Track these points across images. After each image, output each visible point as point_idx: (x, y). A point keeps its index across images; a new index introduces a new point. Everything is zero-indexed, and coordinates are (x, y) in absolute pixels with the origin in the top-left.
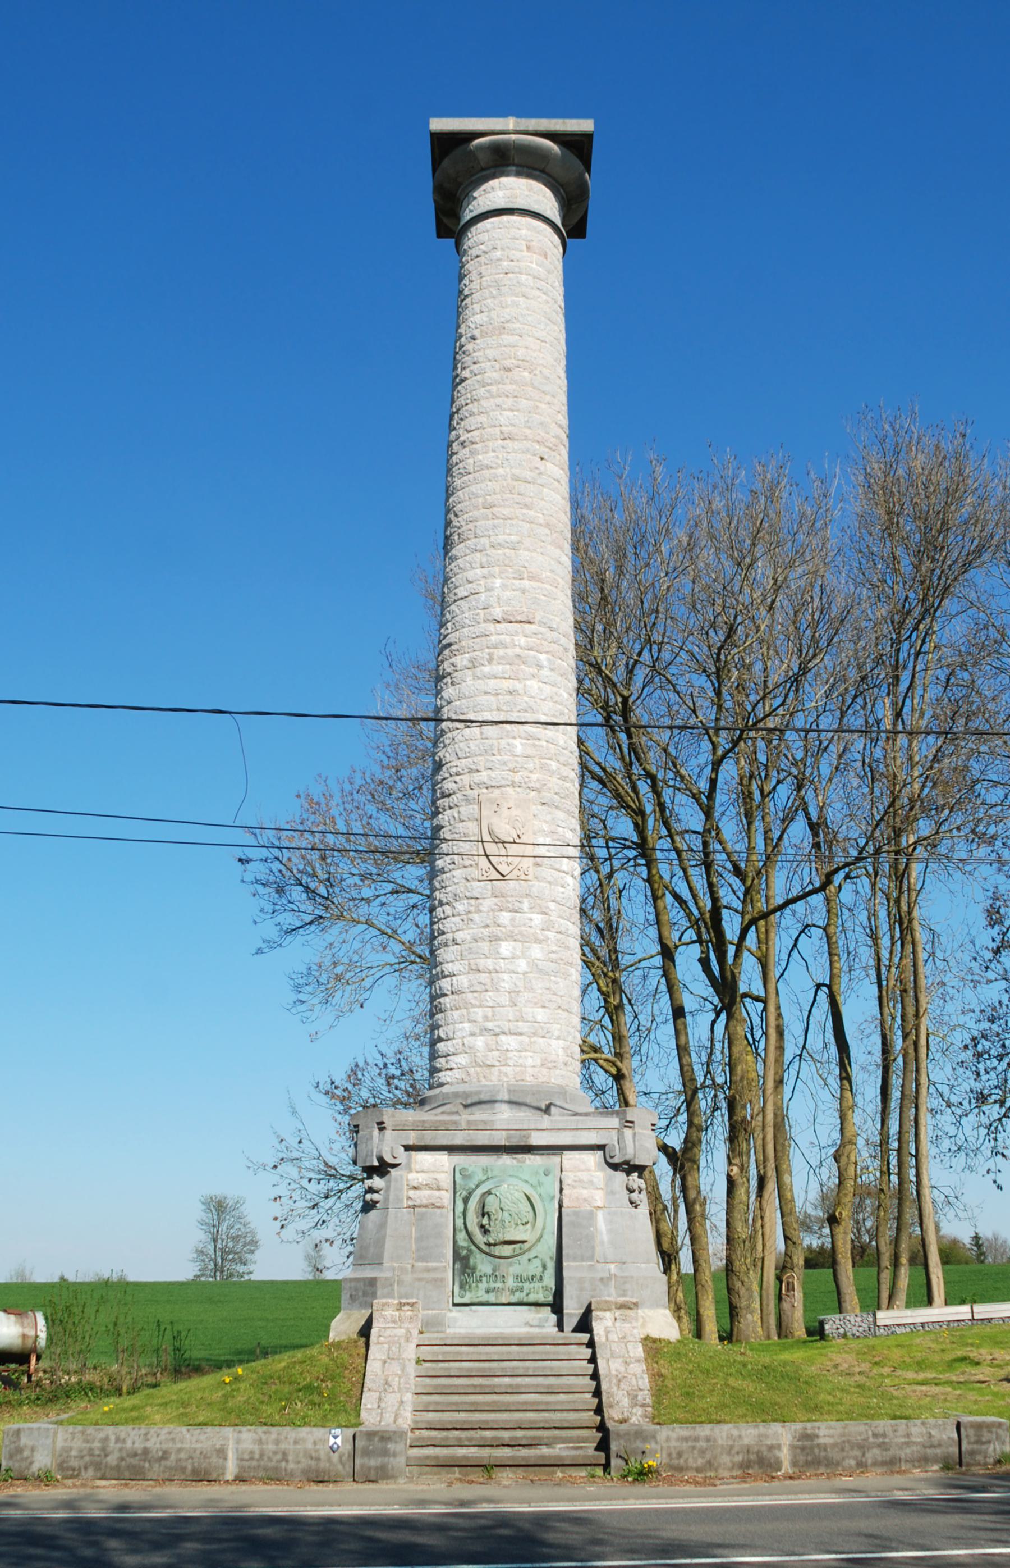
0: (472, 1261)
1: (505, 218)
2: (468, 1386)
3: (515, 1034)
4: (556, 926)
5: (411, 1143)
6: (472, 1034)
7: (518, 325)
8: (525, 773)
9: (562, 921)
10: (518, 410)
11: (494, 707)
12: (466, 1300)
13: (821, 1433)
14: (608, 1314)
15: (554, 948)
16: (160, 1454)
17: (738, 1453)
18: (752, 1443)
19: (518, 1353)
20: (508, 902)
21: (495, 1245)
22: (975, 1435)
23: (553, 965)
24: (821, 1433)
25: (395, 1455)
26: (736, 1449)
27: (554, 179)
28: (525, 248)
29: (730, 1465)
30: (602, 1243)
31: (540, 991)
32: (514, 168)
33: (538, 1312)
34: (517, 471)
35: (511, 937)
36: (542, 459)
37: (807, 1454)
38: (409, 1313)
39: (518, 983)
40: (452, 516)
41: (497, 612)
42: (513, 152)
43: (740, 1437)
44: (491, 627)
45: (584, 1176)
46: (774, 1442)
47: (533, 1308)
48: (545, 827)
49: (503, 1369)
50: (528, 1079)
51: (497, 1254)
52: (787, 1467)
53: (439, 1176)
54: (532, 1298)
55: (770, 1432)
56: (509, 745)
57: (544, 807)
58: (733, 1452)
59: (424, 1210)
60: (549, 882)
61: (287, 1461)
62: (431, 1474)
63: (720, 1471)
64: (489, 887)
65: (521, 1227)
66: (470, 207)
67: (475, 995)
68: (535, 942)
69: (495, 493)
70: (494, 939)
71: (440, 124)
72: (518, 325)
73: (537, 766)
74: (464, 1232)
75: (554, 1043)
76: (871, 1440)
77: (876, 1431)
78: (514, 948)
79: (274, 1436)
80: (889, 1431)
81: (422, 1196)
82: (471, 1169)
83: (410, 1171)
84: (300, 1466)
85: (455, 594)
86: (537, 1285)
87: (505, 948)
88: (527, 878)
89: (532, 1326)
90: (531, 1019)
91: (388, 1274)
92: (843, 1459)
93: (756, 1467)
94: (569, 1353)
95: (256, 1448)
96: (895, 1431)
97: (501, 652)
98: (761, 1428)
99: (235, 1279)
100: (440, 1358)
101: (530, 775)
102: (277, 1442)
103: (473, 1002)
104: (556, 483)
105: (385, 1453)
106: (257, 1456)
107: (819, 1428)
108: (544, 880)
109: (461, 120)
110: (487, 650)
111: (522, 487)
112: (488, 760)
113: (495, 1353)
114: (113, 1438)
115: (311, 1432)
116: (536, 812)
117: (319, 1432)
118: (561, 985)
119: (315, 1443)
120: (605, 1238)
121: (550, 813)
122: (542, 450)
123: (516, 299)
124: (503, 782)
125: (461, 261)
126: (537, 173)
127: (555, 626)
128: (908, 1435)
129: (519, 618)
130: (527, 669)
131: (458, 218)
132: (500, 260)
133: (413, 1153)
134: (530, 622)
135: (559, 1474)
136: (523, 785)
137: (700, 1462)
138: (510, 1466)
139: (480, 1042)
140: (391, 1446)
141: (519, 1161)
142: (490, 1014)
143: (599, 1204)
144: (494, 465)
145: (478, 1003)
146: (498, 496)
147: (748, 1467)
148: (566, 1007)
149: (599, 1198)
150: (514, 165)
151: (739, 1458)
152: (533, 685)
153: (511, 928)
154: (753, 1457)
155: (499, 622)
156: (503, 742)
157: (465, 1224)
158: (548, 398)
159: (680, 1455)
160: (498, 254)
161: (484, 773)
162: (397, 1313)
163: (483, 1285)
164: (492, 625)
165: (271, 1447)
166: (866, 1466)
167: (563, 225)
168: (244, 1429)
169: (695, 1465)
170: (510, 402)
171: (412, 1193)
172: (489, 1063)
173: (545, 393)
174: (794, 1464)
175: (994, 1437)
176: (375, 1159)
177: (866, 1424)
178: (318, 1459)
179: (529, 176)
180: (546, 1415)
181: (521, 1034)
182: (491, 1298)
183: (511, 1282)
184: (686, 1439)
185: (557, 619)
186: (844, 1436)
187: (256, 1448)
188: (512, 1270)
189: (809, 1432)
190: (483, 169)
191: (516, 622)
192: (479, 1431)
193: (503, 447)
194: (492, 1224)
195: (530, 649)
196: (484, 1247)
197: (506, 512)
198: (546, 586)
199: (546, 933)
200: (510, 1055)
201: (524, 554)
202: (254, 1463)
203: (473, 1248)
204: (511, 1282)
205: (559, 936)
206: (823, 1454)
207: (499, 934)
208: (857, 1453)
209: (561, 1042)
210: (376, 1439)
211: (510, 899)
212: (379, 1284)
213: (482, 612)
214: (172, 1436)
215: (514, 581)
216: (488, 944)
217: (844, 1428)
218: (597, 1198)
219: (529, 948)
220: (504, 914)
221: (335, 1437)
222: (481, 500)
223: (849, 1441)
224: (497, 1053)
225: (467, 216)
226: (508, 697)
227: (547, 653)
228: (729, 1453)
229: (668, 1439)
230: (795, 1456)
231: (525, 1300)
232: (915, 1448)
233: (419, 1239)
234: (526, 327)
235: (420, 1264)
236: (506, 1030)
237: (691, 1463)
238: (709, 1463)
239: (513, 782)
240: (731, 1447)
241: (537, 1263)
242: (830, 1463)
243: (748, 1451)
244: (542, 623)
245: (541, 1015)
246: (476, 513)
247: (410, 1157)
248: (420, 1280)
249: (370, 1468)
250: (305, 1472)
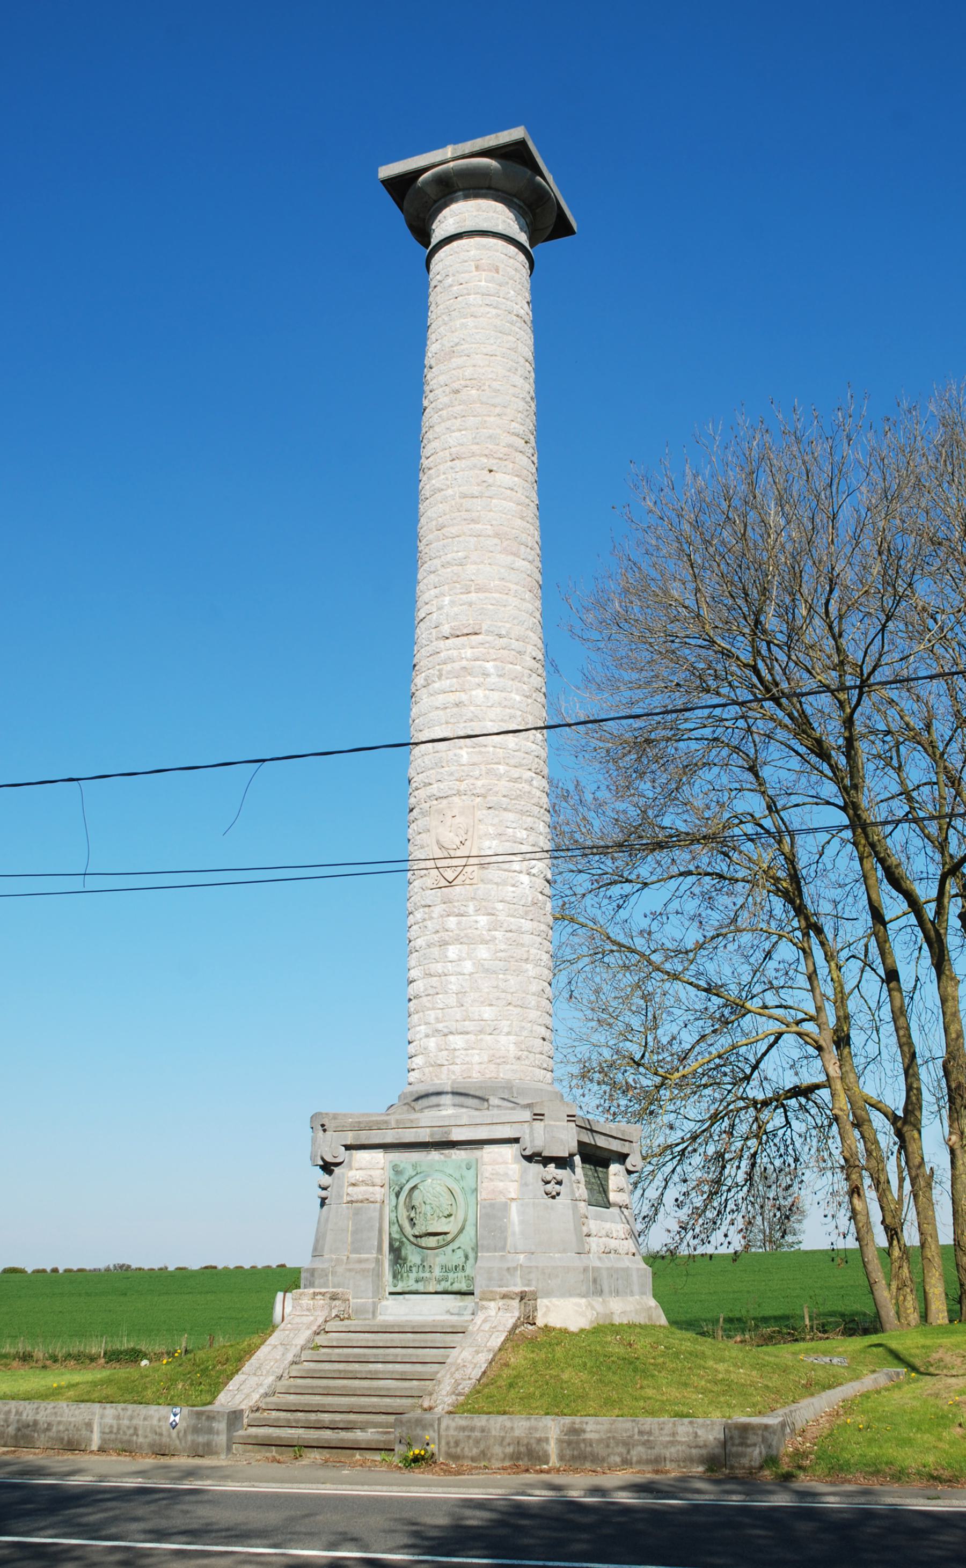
0: (403, 1252)
1: (455, 244)
2: (334, 1371)
3: (461, 1033)
4: (505, 925)
5: (349, 1143)
6: (427, 1036)
7: (466, 346)
8: (472, 781)
9: (512, 920)
10: (465, 429)
11: (443, 721)
12: (398, 1289)
13: (589, 1428)
14: (492, 1304)
15: (503, 947)
16: (46, 1425)
17: (509, 1444)
18: (523, 1435)
19: (401, 1340)
20: (454, 907)
21: (421, 1237)
22: (740, 1437)
23: (502, 963)
24: (589, 1428)
25: (218, 1433)
26: (507, 1440)
27: (503, 192)
28: (474, 269)
29: (501, 1455)
30: (514, 1233)
31: (487, 990)
32: (460, 193)
33: (462, 1300)
34: (464, 489)
35: (458, 940)
36: (491, 471)
37: (573, 1449)
38: (322, 1302)
39: (464, 984)
41: (446, 629)
42: (455, 179)
43: (512, 1428)
44: (442, 644)
45: (501, 1169)
46: (543, 1435)
47: (458, 1296)
48: (491, 830)
49: (375, 1355)
50: (474, 1075)
51: (423, 1245)
52: (554, 1461)
53: (372, 1173)
54: (456, 1287)
55: (541, 1424)
56: (455, 755)
57: (490, 811)
58: (505, 1443)
59: (360, 1205)
60: (496, 883)
61: (137, 1435)
62: (253, 1452)
63: (493, 1461)
64: (439, 894)
65: (444, 1219)
67: (429, 998)
68: (481, 943)
69: (445, 514)
70: (444, 944)
71: (387, 171)
72: (466, 346)
73: (483, 772)
74: (396, 1225)
75: (503, 1039)
76: (636, 1437)
77: (642, 1428)
78: (460, 951)
79: (129, 1413)
80: (655, 1428)
81: (358, 1192)
82: (402, 1166)
83: (351, 1168)
84: (148, 1440)
86: (460, 1274)
87: (453, 951)
88: (472, 882)
89: (452, 1314)
90: (476, 1018)
91: (326, 1265)
92: (608, 1455)
93: (526, 1459)
94: (444, 1342)
95: (114, 1422)
96: (662, 1429)
97: (448, 667)
98: (533, 1420)
99: (785, 1249)
100: (335, 1344)
101: (476, 782)
102: (131, 1418)
103: (428, 1005)
104: (509, 491)
105: (210, 1431)
106: (115, 1430)
107: (587, 1423)
108: (490, 882)
109: (405, 161)
110: (438, 667)
111: (467, 503)
112: (438, 773)
113: (381, 1340)
114: (14, 1411)
115: (157, 1410)
116: (481, 817)
117: (164, 1410)
118: (512, 982)
119: (159, 1420)
120: (517, 1229)
121: (497, 816)
122: (492, 463)
123: (463, 321)
124: (450, 792)
126: (484, 191)
127: (504, 632)
128: (674, 1434)
129: (465, 631)
130: (472, 679)
132: (451, 286)
133: (354, 1152)
134: (476, 634)
135: (358, 1456)
136: (469, 792)
137: (475, 1451)
138: (317, 1447)
139: (432, 1043)
140: (215, 1425)
141: (446, 1156)
142: (440, 1016)
143: (513, 1195)
144: (444, 487)
145: (431, 1006)
146: (448, 516)
147: (518, 1459)
148: (519, 1003)
149: (513, 1190)
150: (460, 190)
151: (509, 1450)
152: (479, 693)
153: (458, 932)
154: (523, 1449)
155: (447, 638)
156: (451, 753)
158: (498, 410)
159: (457, 1444)
160: (449, 280)
161: (435, 786)
162: (311, 1302)
163: (413, 1275)
164: (442, 642)
165: (126, 1422)
166: (631, 1464)
168: (108, 1405)
169: (470, 1454)
170: (458, 422)
171: (351, 1190)
172: (439, 1062)
173: (495, 406)
174: (561, 1458)
175: (760, 1440)
176: (319, 1158)
177: (634, 1421)
178: (161, 1435)
179: (477, 196)
180: (388, 1400)
181: (468, 1033)
182: (420, 1287)
183: (437, 1272)
184: (463, 1429)
185: (508, 625)
186: (610, 1432)
187: (114, 1422)
188: (438, 1260)
189: (577, 1426)
190: (435, 202)
191: (463, 635)
192: (319, 1414)
193: (452, 468)
195: (477, 659)
196: (412, 1239)
197: (454, 530)
198: (494, 595)
199: (493, 933)
200: (457, 1053)
201: (471, 568)
202: (113, 1436)
203: (404, 1239)
204: (437, 1272)
205: (510, 934)
206: (589, 1449)
207: (447, 939)
208: (621, 1449)
209: (512, 1038)
210: (204, 1418)
211: (456, 904)
212: (316, 1274)
213: (434, 631)
214: (56, 1410)
215: (462, 596)
216: (438, 948)
217: (612, 1424)
218: (511, 1190)
219: (475, 949)
220: (451, 918)
221: (175, 1415)
222: (434, 523)
223: (614, 1438)
224: (445, 1053)
225: (434, 241)
226: (455, 710)
227: (495, 660)
228: (501, 1444)
229: (448, 1428)
230: (562, 1450)
231: (450, 1289)
232: (679, 1448)
233: (355, 1232)
234: (474, 346)
235: (354, 1256)
236: (454, 1030)
237: (467, 1452)
238: (483, 1453)
239: (459, 791)
240: (503, 1438)
241: (460, 1253)
242: (595, 1459)
243: (518, 1443)
244: (489, 632)
245: (488, 1013)
246: (430, 537)
247: (351, 1155)
248: (350, 1270)
249: (198, 1444)
250: (151, 1445)
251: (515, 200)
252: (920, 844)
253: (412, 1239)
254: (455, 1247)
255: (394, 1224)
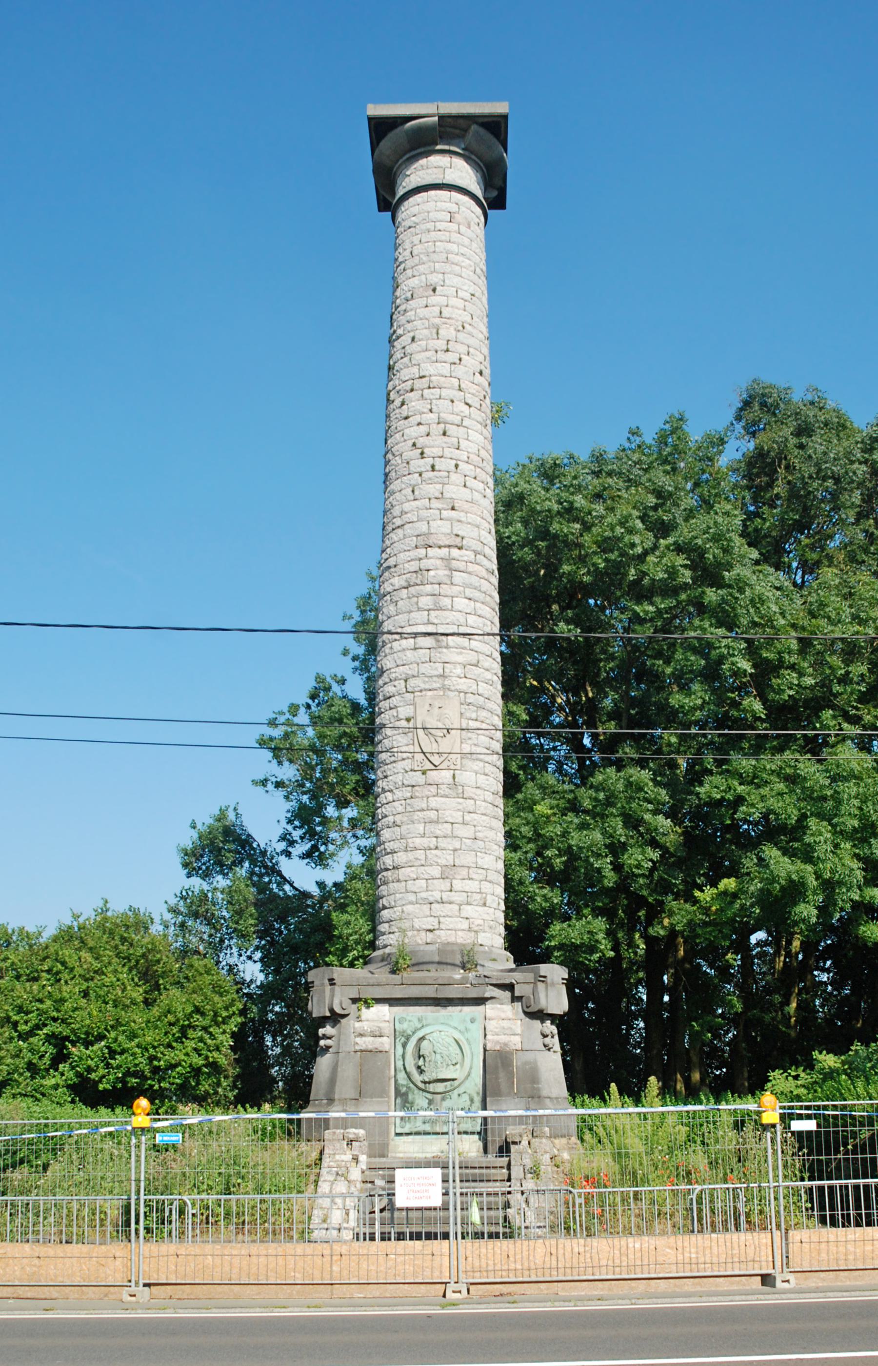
0: (410, 1097)
1: (432, 193)
21: (429, 1083)
40: (389, 456)
51: (431, 1090)
65: (452, 1067)
66: (404, 184)
85: (393, 523)
125: (396, 232)
131: (394, 194)
157: (404, 1065)
167: (485, 198)
194: (427, 1065)
196: (422, 1086)
203: (411, 1085)
225: (400, 192)
241: (466, 1097)
251: (473, 157)
252: (530, 977)
253: (422, 1086)
254: (461, 1092)
255: (400, 1071)
